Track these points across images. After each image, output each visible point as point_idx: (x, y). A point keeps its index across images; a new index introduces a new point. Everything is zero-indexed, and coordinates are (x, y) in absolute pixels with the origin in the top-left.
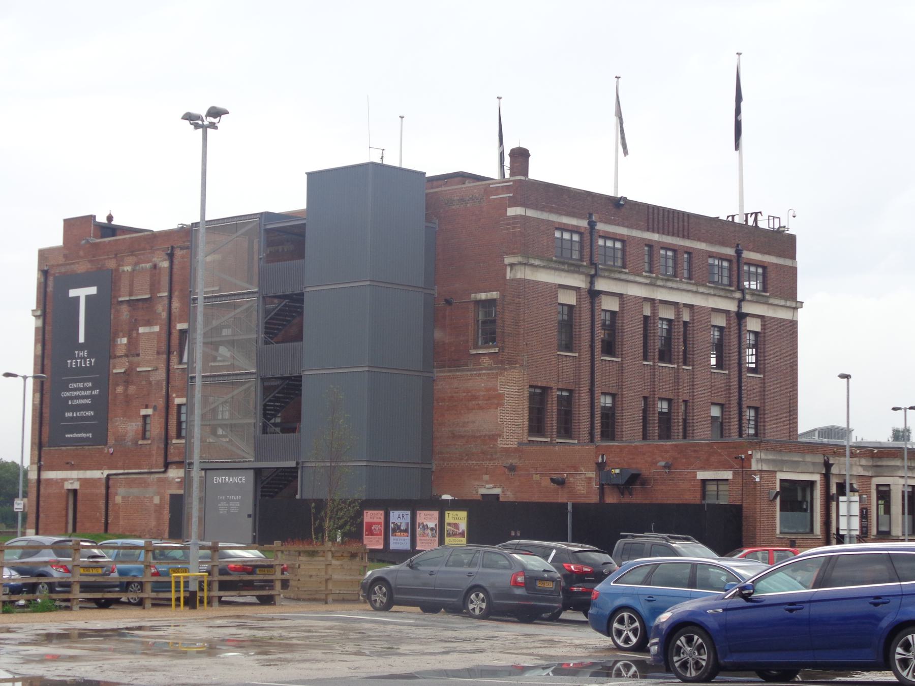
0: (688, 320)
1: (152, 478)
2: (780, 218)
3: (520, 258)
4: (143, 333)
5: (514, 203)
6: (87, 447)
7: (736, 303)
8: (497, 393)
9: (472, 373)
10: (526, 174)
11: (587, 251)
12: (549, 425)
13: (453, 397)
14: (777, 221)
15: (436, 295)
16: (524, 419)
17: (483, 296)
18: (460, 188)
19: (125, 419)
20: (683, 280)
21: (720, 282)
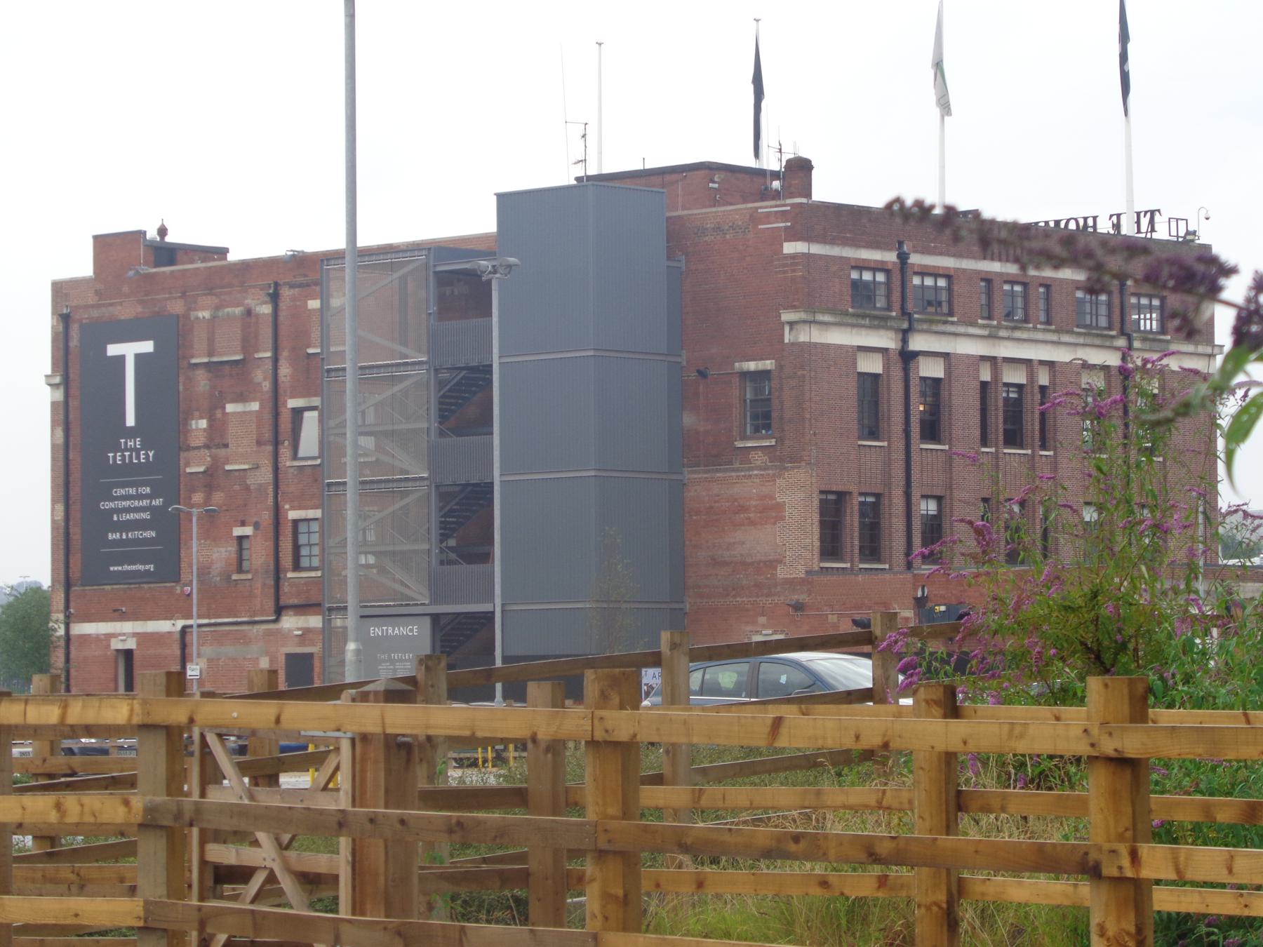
0: (1047, 384)
1: (255, 631)
3: (802, 313)
4: (234, 413)
5: (793, 236)
6: (146, 586)
8: (774, 502)
9: (738, 474)
10: (808, 194)
11: (896, 296)
12: (849, 545)
13: (711, 508)
14: (1182, 224)
15: (684, 363)
16: (812, 538)
17: (752, 366)
18: (715, 212)
19: (208, 542)
20: (1039, 326)
21: (1094, 324)
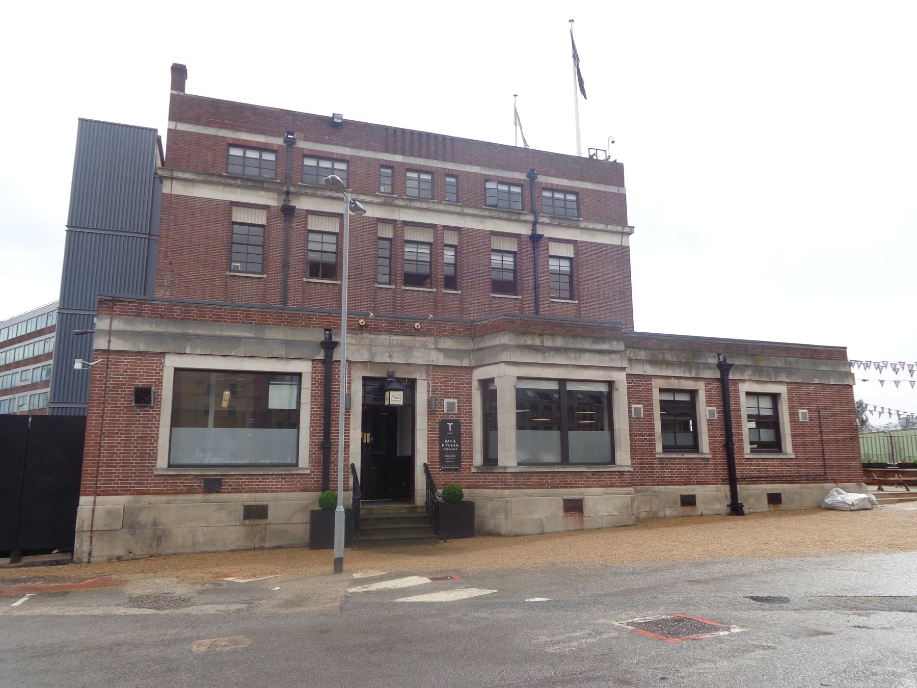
2: (606, 151)
7: (530, 227)
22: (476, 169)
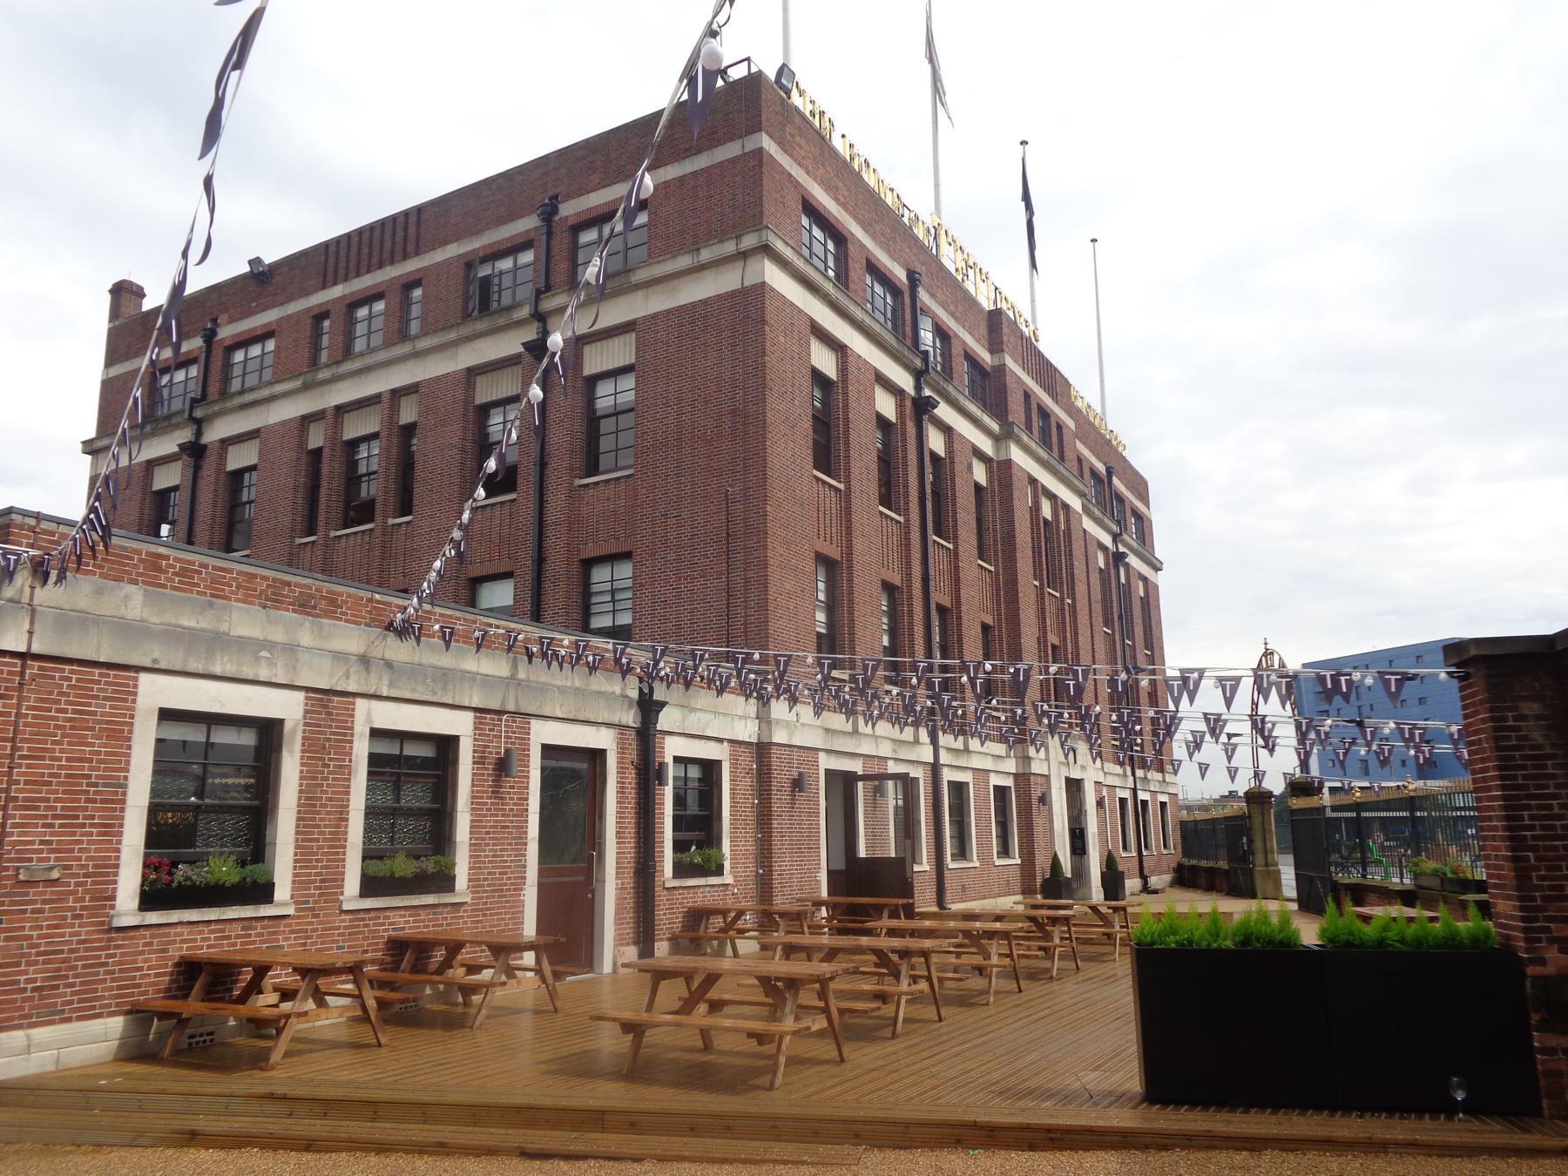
22: (453, 250)
